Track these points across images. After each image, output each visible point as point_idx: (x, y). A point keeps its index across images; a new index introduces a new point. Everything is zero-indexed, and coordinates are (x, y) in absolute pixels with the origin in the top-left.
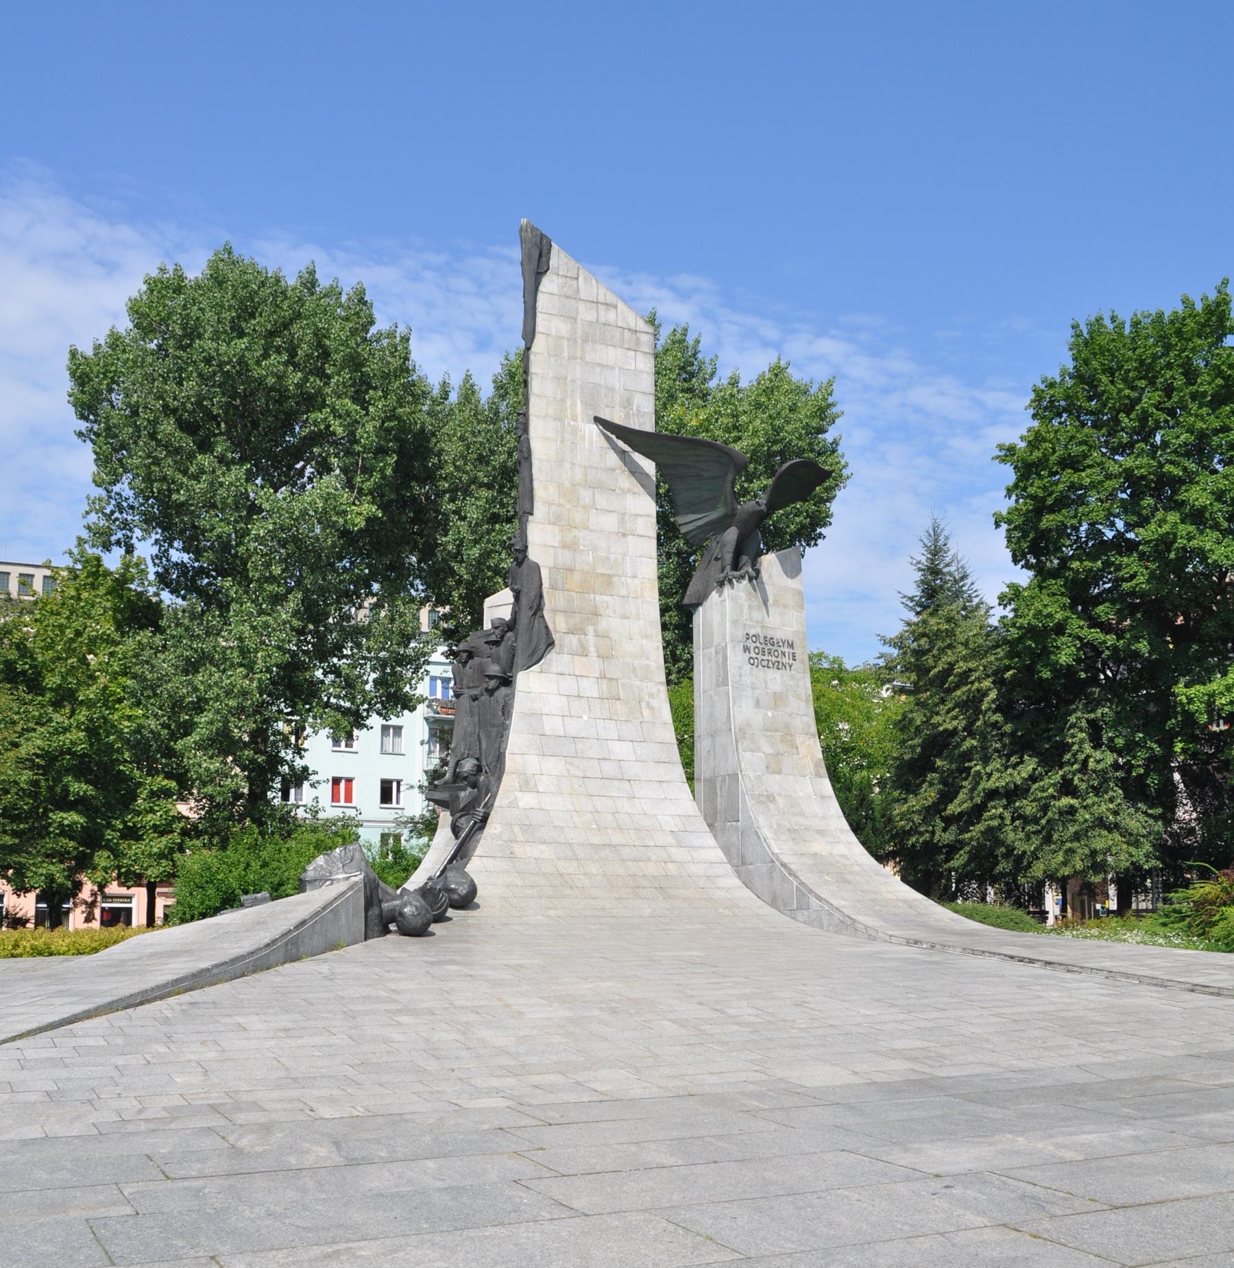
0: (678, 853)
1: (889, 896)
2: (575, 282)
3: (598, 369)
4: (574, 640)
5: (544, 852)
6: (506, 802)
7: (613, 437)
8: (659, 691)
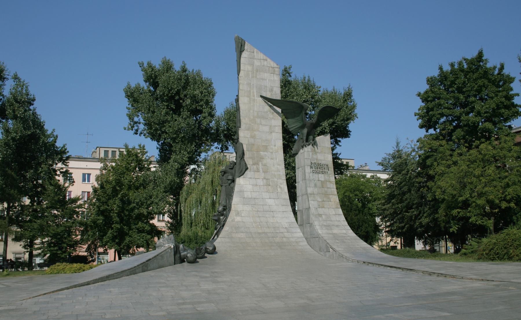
0: (286, 234)
1: (357, 246)
4: (255, 167)
5: (242, 235)
6: (231, 220)
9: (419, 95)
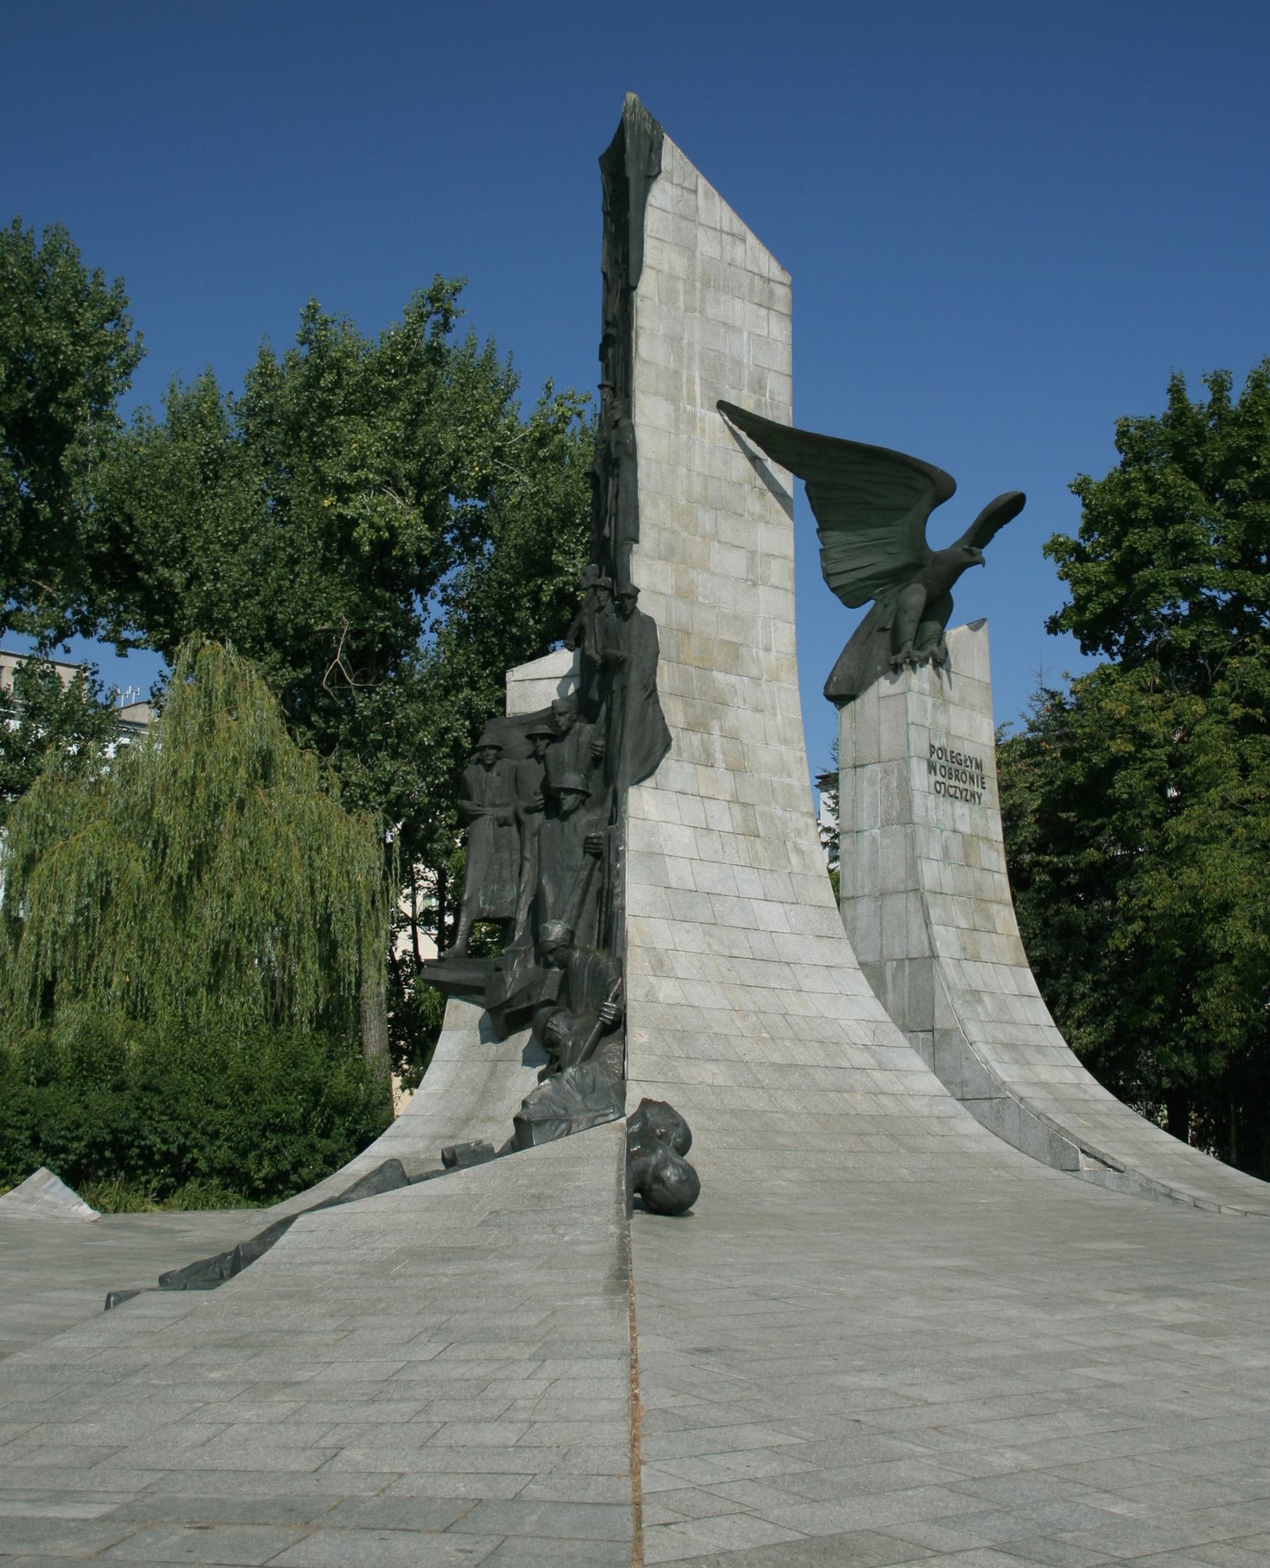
2: (692, 196)
3: (722, 331)
4: (695, 739)
7: (743, 434)
8: (807, 826)
9: (1081, 488)
